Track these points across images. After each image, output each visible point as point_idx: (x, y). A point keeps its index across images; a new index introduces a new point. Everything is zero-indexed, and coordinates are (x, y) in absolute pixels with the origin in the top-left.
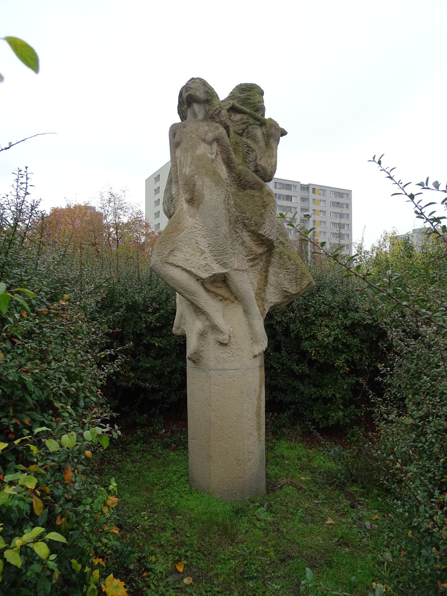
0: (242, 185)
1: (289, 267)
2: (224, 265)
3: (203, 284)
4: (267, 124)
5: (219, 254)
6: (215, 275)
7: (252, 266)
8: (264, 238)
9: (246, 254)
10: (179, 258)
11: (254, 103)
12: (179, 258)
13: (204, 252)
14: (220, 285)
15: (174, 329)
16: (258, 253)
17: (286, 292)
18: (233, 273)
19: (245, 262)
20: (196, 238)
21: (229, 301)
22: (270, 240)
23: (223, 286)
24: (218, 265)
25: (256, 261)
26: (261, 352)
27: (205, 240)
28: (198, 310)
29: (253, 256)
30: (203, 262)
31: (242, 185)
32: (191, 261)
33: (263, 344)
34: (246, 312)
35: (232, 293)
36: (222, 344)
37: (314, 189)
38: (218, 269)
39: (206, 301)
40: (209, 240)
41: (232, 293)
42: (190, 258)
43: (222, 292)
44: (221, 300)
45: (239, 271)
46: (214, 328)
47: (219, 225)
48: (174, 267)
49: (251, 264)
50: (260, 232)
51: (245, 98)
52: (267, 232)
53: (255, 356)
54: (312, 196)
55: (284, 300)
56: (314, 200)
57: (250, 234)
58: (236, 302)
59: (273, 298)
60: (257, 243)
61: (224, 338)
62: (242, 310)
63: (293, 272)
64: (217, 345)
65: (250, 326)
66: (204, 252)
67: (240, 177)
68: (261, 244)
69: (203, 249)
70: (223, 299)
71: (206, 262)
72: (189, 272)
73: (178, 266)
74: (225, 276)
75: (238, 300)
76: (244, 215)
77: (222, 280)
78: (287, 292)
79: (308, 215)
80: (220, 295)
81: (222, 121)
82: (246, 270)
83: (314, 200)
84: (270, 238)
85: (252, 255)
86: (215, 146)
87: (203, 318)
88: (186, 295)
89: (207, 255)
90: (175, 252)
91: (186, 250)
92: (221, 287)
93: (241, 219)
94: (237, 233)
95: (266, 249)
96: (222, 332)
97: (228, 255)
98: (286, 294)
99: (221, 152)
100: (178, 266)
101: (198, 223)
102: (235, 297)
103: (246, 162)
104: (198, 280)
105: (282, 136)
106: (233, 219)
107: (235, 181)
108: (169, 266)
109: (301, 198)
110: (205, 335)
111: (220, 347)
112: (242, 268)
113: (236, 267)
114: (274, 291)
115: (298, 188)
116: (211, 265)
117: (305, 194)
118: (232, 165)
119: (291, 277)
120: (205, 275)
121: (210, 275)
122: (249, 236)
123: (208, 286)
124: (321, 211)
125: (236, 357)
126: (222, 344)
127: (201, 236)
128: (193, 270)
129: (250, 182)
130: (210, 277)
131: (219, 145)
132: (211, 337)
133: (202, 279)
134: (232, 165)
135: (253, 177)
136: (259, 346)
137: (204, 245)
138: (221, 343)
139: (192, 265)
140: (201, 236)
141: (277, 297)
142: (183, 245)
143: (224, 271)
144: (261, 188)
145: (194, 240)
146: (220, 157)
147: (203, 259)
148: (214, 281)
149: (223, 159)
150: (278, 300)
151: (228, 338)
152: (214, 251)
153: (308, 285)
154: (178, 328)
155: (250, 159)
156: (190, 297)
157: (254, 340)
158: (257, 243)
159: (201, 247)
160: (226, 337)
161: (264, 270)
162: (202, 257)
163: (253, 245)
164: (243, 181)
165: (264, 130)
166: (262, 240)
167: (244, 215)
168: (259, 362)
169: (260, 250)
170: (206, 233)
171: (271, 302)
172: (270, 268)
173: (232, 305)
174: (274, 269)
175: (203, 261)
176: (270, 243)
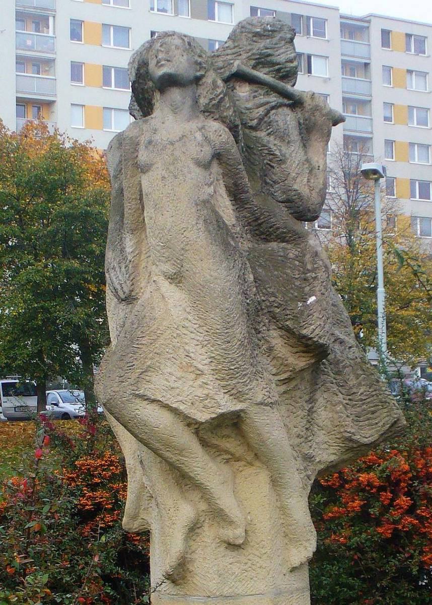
0: (263, 233)
1: (354, 390)
2: (238, 396)
3: (197, 433)
4: (306, 105)
5: (230, 377)
6: (222, 415)
7: (285, 393)
8: (310, 342)
9: (274, 371)
10: (156, 386)
11: (279, 64)
12: (156, 386)
13: (201, 373)
14: (226, 432)
15: (125, 520)
16: (298, 368)
17: (350, 440)
18: (253, 411)
19: (274, 385)
20: (187, 348)
21: (243, 463)
22: (322, 345)
23: (233, 435)
24: (227, 396)
25: (293, 383)
26: (304, 560)
27: (204, 350)
28: (183, 479)
29: (289, 373)
30: (200, 392)
31: (263, 233)
32: (177, 391)
33: (307, 545)
34: (276, 482)
35: (249, 446)
36: (232, 546)
37: (386, 35)
38: (228, 405)
39: (201, 464)
40: (212, 352)
41: (249, 446)
42: (176, 385)
43: (232, 445)
44: (227, 461)
45: (266, 405)
46: (219, 515)
47: (232, 324)
48: (146, 402)
49: (283, 388)
50: (304, 332)
51: (260, 54)
52: (317, 332)
53: (293, 570)
54: (379, 57)
55: (345, 457)
56: (389, 143)
57: (284, 332)
58: (257, 464)
59: (327, 453)
60: (295, 350)
61: (235, 534)
62: (268, 480)
63: (362, 400)
64: (222, 549)
65: (283, 509)
66: (201, 373)
67: (257, 219)
68: (304, 352)
69: (200, 367)
70: (232, 459)
71: (206, 392)
72: (175, 411)
73: (154, 401)
74: (239, 416)
75: (261, 461)
76: (273, 299)
77: (233, 423)
78: (351, 440)
79: (375, 172)
80: (227, 452)
81: (226, 117)
82: (275, 403)
83: (388, 69)
84: (321, 341)
85: (285, 372)
86: (216, 168)
87: (195, 496)
88: (168, 454)
89: (209, 378)
90: (149, 374)
91: (169, 370)
92: (228, 437)
93: (267, 307)
94: (260, 332)
95: (313, 361)
96: (231, 523)
97: (246, 378)
98: (350, 444)
99: (224, 175)
100: (154, 401)
101: (190, 318)
102: (256, 455)
103: (266, 183)
104: (189, 425)
105: (335, 125)
106: (252, 308)
107: (249, 224)
108: (138, 401)
109: (343, 26)
110: (197, 531)
111: (228, 552)
112: (270, 400)
113: (259, 400)
114: (326, 439)
115: (333, 30)
116: (216, 397)
117: (356, 50)
118: (243, 196)
119: (358, 409)
120: (203, 416)
121: (214, 416)
122: (281, 336)
123: (207, 436)
124: (410, 72)
125: (259, 570)
126: (232, 546)
127: (195, 342)
128: (182, 407)
129: (278, 228)
130: (213, 419)
131: (220, 164)
132: (209, 533)
133: (197, 422)
134: (243, 196)
135: (282, 217)
136: (302, 549)
137: (201, 359)
138: (229, 544)
139: (180, 398)
140: (195, 342)
141: (331, 451)
142: (162, 361)
143: (239, 407)
144: (297, 238)
145: (182, 350)
146: (222, 186)
147: (201, 386)
148: (219, 426)
149: (226, 187)
150: (333, 458)
151: (244, 534)
152: (220, 370)
153: (392, 425)
154: (134, 517)
155: (275, 178)
156: (173, 458)
157: (289, 536)
158: (295, 350)
159: (195, 363)
160: (240, 531)
161: (307, 398)
162: (199, 382)
163: (289, 355)
164: (264, 225)
165: (300, 115)
166: (307, 346)
167: (273, 299)
168: (302, 581)
169: (301, 362)
170: (207, 338)
171: (319, 462)
172: (318, 395)
173: (249, 470)
174: (325, 395)
175: (201, 390)
176: (321, 350)
